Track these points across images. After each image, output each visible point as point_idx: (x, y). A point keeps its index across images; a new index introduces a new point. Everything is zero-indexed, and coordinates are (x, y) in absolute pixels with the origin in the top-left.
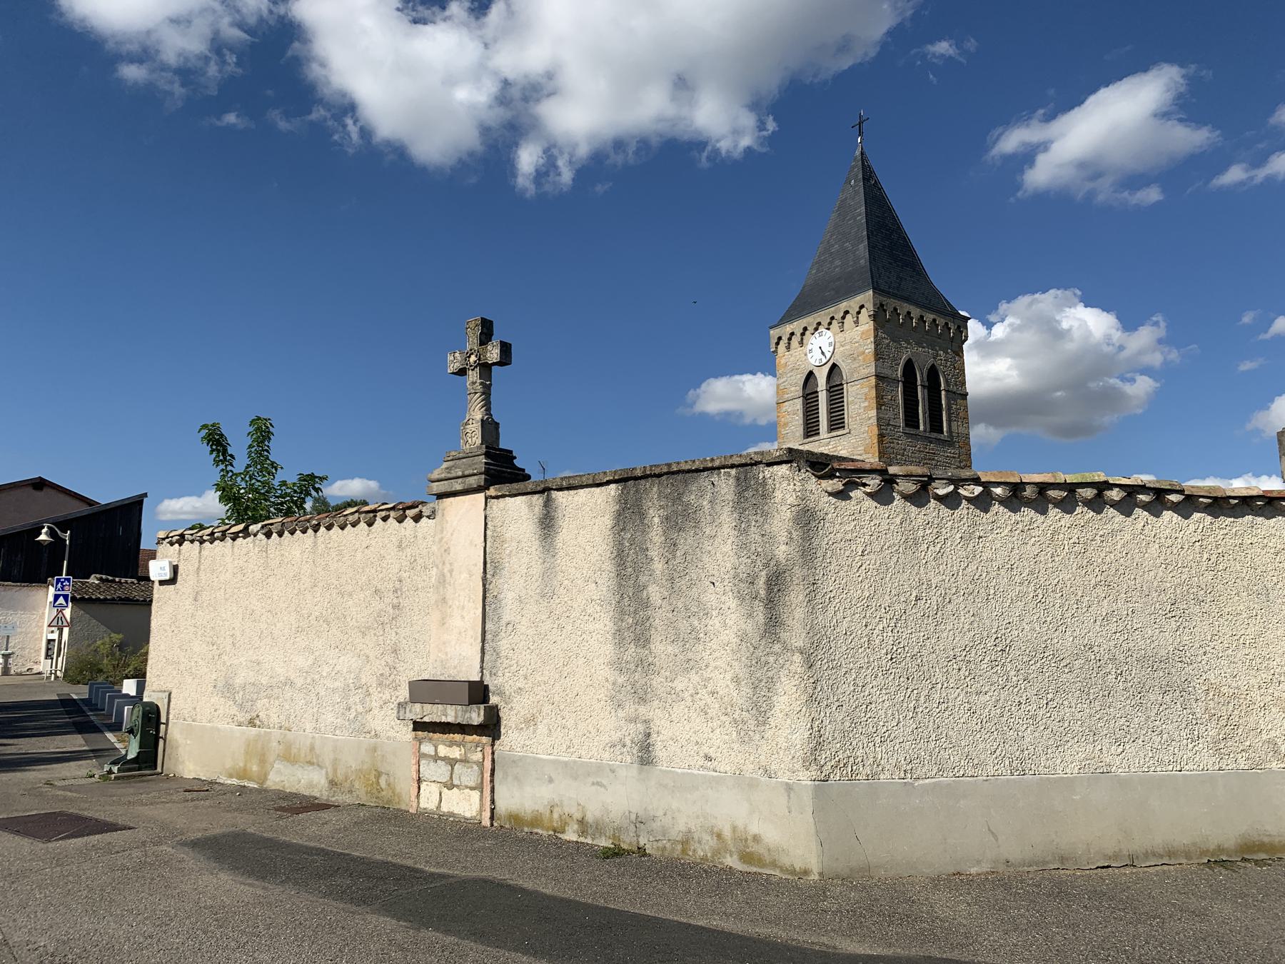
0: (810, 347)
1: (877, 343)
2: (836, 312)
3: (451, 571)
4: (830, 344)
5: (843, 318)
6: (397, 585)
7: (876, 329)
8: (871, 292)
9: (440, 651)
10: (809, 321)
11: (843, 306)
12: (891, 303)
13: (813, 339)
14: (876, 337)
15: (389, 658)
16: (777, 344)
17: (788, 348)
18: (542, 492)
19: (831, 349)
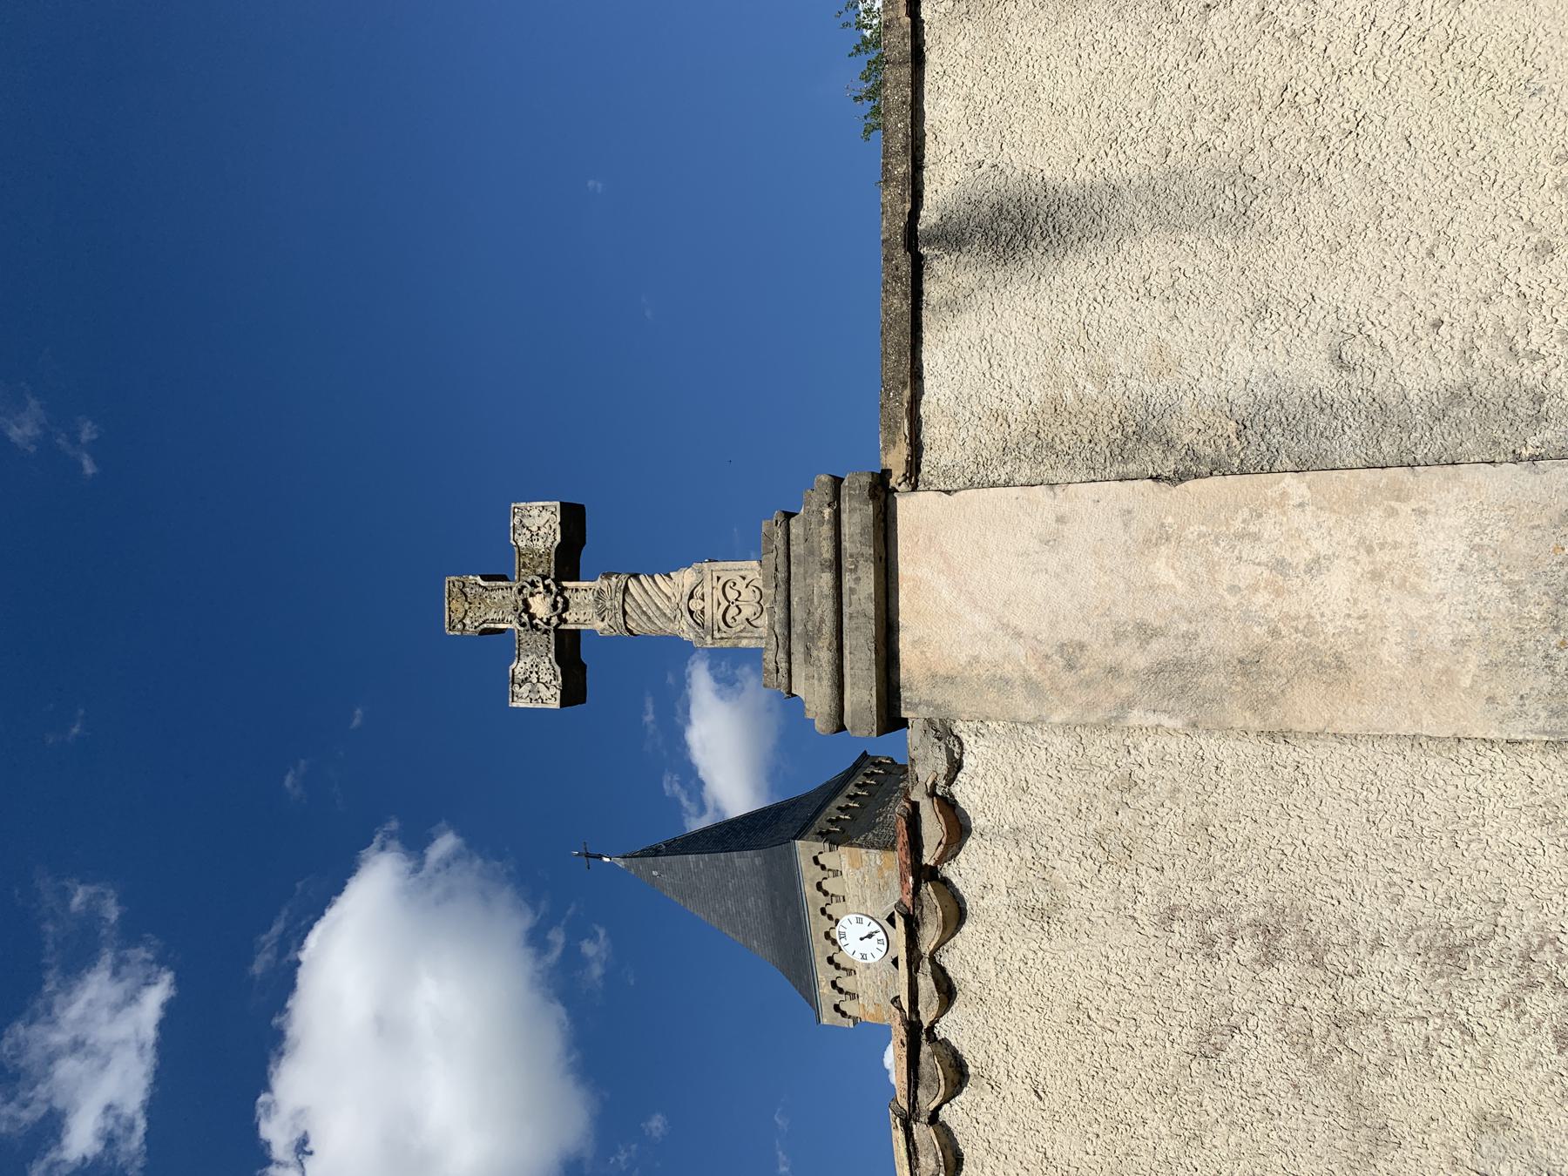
0: (857, 957)
3: (1146, 633)
4: (859, 921)
5: (826, 893)
6: (1182, 934)
7: (851, 845)
8: (798, 843)
9: (1447, 679)
10: (820, 950)
11: (809, 890)
12: (821, 823)
13: (848, 950)
14: (861, 846)
15: (1484, 994)
16: (844, 1014)
17: (854, 996)
18: (918, 264)
19: (866, 920)
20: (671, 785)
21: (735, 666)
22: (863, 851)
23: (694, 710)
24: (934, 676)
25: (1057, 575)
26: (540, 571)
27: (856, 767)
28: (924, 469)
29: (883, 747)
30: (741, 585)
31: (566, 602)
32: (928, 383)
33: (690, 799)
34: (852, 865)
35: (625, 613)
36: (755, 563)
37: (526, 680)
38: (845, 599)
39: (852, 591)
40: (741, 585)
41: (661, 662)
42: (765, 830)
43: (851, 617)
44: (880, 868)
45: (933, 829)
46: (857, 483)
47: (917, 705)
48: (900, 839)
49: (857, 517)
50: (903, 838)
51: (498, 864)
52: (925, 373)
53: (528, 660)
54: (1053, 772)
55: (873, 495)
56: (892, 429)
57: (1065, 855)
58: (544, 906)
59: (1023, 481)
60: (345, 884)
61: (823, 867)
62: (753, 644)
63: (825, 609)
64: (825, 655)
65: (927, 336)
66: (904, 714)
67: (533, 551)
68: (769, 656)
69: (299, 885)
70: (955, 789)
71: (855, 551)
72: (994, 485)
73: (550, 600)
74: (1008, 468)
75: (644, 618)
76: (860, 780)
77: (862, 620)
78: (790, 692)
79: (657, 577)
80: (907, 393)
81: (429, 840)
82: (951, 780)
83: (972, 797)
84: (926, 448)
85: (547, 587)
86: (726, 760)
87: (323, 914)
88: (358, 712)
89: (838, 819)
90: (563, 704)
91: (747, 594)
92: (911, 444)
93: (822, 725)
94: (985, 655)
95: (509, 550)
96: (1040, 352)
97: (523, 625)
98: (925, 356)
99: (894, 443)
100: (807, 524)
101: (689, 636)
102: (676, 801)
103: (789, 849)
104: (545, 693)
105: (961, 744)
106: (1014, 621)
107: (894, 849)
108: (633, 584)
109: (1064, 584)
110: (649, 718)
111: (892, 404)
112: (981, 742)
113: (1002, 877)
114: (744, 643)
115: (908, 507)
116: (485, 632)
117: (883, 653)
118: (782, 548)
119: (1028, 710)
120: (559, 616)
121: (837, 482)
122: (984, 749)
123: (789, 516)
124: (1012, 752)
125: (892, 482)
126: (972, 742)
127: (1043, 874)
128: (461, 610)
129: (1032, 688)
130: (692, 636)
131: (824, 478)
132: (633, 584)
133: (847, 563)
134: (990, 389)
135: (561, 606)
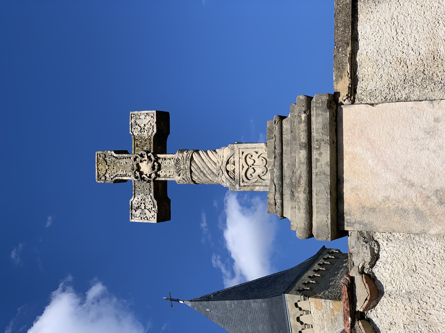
1: (327, 298)
2: (296, 329)
5: (302, 323)
7: (316, 297)
8: (286, 295)
11: (292, 321)
12: (299, 285)
14: (321, 298)
20: (216, 262)
21: (251, 197)
22: (323, 300)
23: (229, 221)
24: (363, 208)
25: (434, 152)
26: (145, 148)
27: (319, 254)
28: (359, 91)
29: (336, 245)
30: (255, 156)
31: (159, 166)
32: (361, 43)
33: (226, 269)
34: (317, 308)
35: (191, 172)
36: (263, 145)
37: (138, 208)
38: (314, 165)
39: (317, 160)
40: (255, 156)
41: (210, 198)
42: (269, 288)
43: (317, 175)
44: (332, 310)
45: (362, 292)
46: (320, 100)
47: (354, 224)
48: (344, 297)
49: (320, 119)
50: (345, 296)
51: (125, 301)
52: (360, 37)
53: (139, 197)
54: (431, 261)
55: (329, 106)
56: (340, 69)
57: (437, 307)
58: (149, 324)
59: (416, 98)
60: (44, 309)
61: (300, 309)
62: (262, 189)
63: (302, 170)
64: (302, 196)
65: (361, 16)
66: (346, 228)
67: (141, 138)
68: (271, 196)
69: (19, 309)
70: (375, 270)
71: (319, 138)
72: (399, 100)
73: (150, 164)
74: (407, 91)
75: (202, 175)
76: (321, 261)
77: (323, 176)
78: (282, 216)
79: (209, 152)
80: (349, 49)
81: (88, 287)
82: (372, 265)
83: (384, 274)
84: (360, 80)
85: (149, 157)
86: (247, 250)
87: (32, 325)
88: (50, 218)
89: (309, 283)
90: (158, 221)
91: (259, 162)
92: (351, 78)
93: (300, 234)
94: (392, 196)
95: (129, 137)
96: (425, 26)
97: (137, 178)
98: (360, 28)
99: (342, 77)
100: (292, 123)
101: (226, 184)
102: (218, 270)
103: (281, 299)
104: (149, 215)
105: (379, 245)
106: (410, 177)
107: (340, 300)
108: (195, 156)
109: (438, 157)
110: (204, 225)
111: (340, 55)
112: (390, 244)
113: (401, 318)
114: (257, 189)
115: (349, 113)
116: (116, 181)
117: (334, 195)
118: (278, 136)
119: (417, 227)
120: (156, 173)
121: (309, 99)
122: (391, 248)
123: (282, 118)
124: (407, 250)
125: (340, 99)
126: (385, 244)
127: (424, 317)
128: (104, 169)
129: (419, 214)
130: (228, 184)
131: (302, 97)
132: (195, 156)
133: (314, 145)
134: (397, 47)
135: (157, 168)
